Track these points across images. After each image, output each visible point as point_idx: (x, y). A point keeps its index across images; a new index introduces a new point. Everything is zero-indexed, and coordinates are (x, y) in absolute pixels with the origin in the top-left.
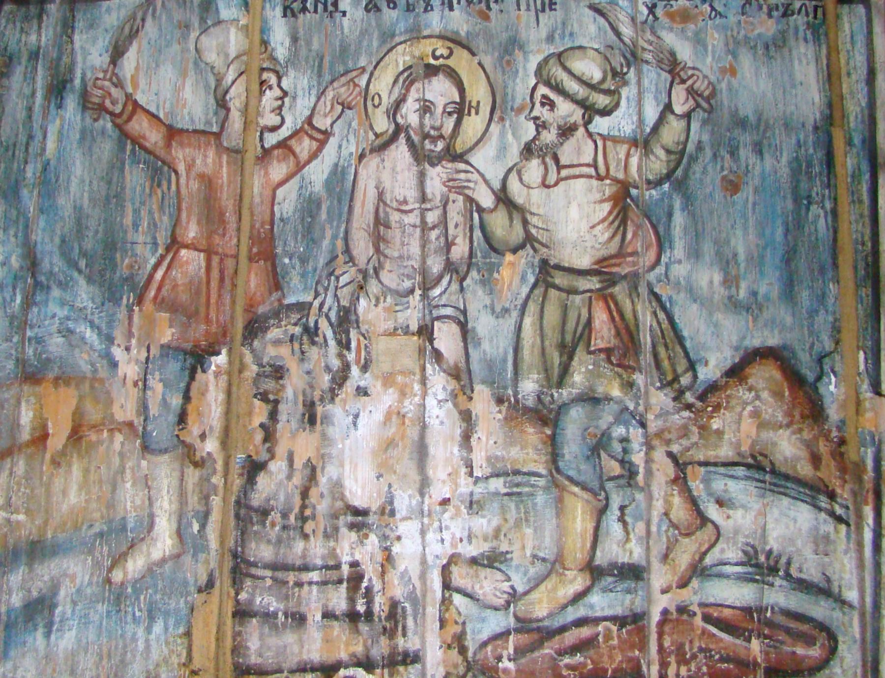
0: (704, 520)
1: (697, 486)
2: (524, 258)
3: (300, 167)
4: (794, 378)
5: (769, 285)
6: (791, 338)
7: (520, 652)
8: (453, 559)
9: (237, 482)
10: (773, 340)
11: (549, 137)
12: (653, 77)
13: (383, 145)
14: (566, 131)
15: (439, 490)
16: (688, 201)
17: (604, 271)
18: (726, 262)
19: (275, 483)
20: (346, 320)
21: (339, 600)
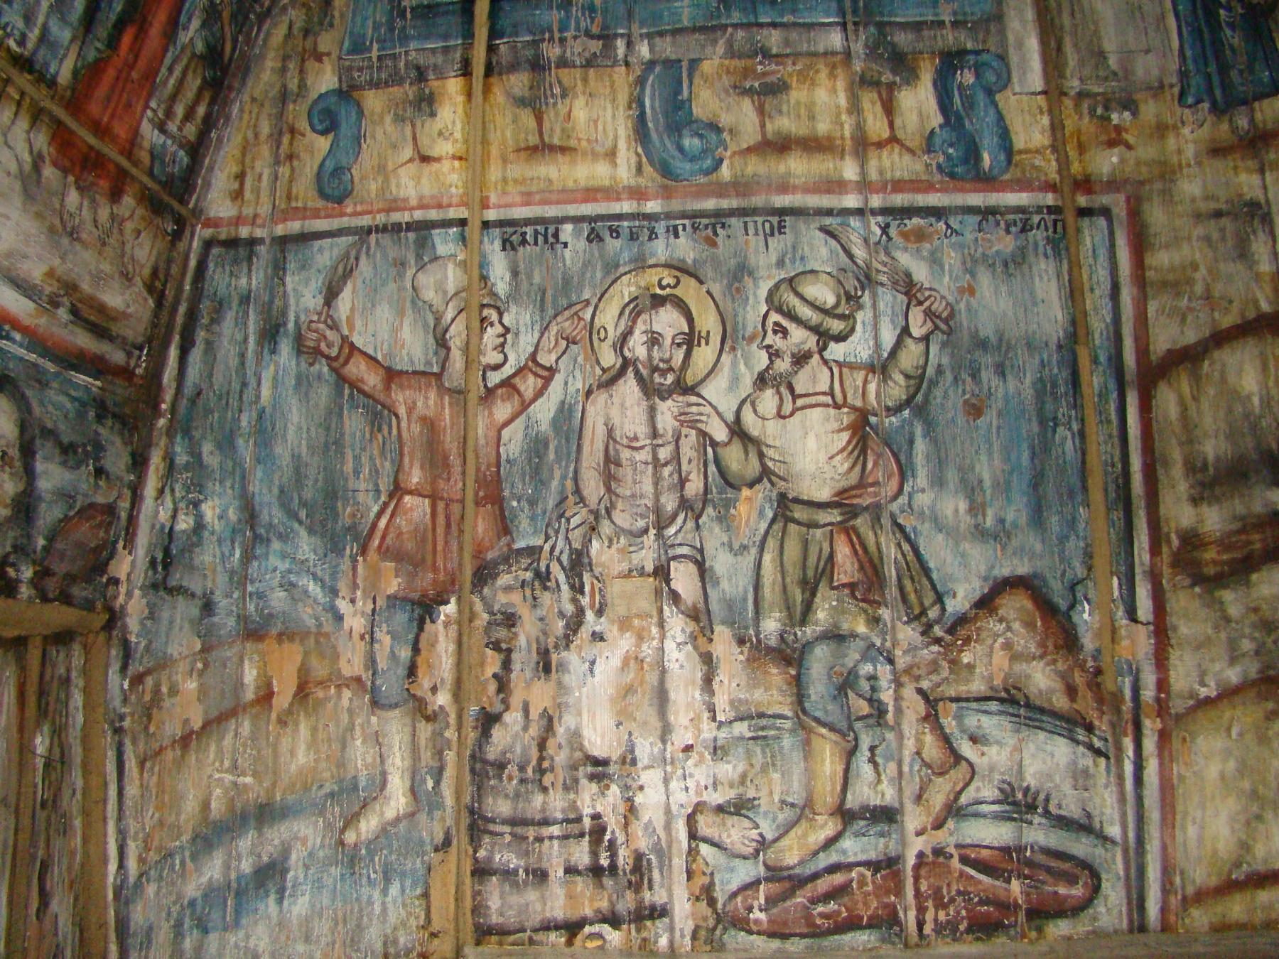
0: (958, 758)
1: (949, 723)
2: (761, 493)
3: (525, 406)
4: (1046, 606)
5: (1017, 511)
6: (1041, 565)
7: (771, 901)
8: (699, 807)
9: (472, 735)
10: (1023, 569)
11: (783, 365)
12: (888, 299)
13: (610, 380)
14: (801, 359)
15: (682, 736)
16: (929, 426)
17: (844, 502)
18: (971, 489)
19: (510, 736)
20: (578, 563)
21: (581, 854)
